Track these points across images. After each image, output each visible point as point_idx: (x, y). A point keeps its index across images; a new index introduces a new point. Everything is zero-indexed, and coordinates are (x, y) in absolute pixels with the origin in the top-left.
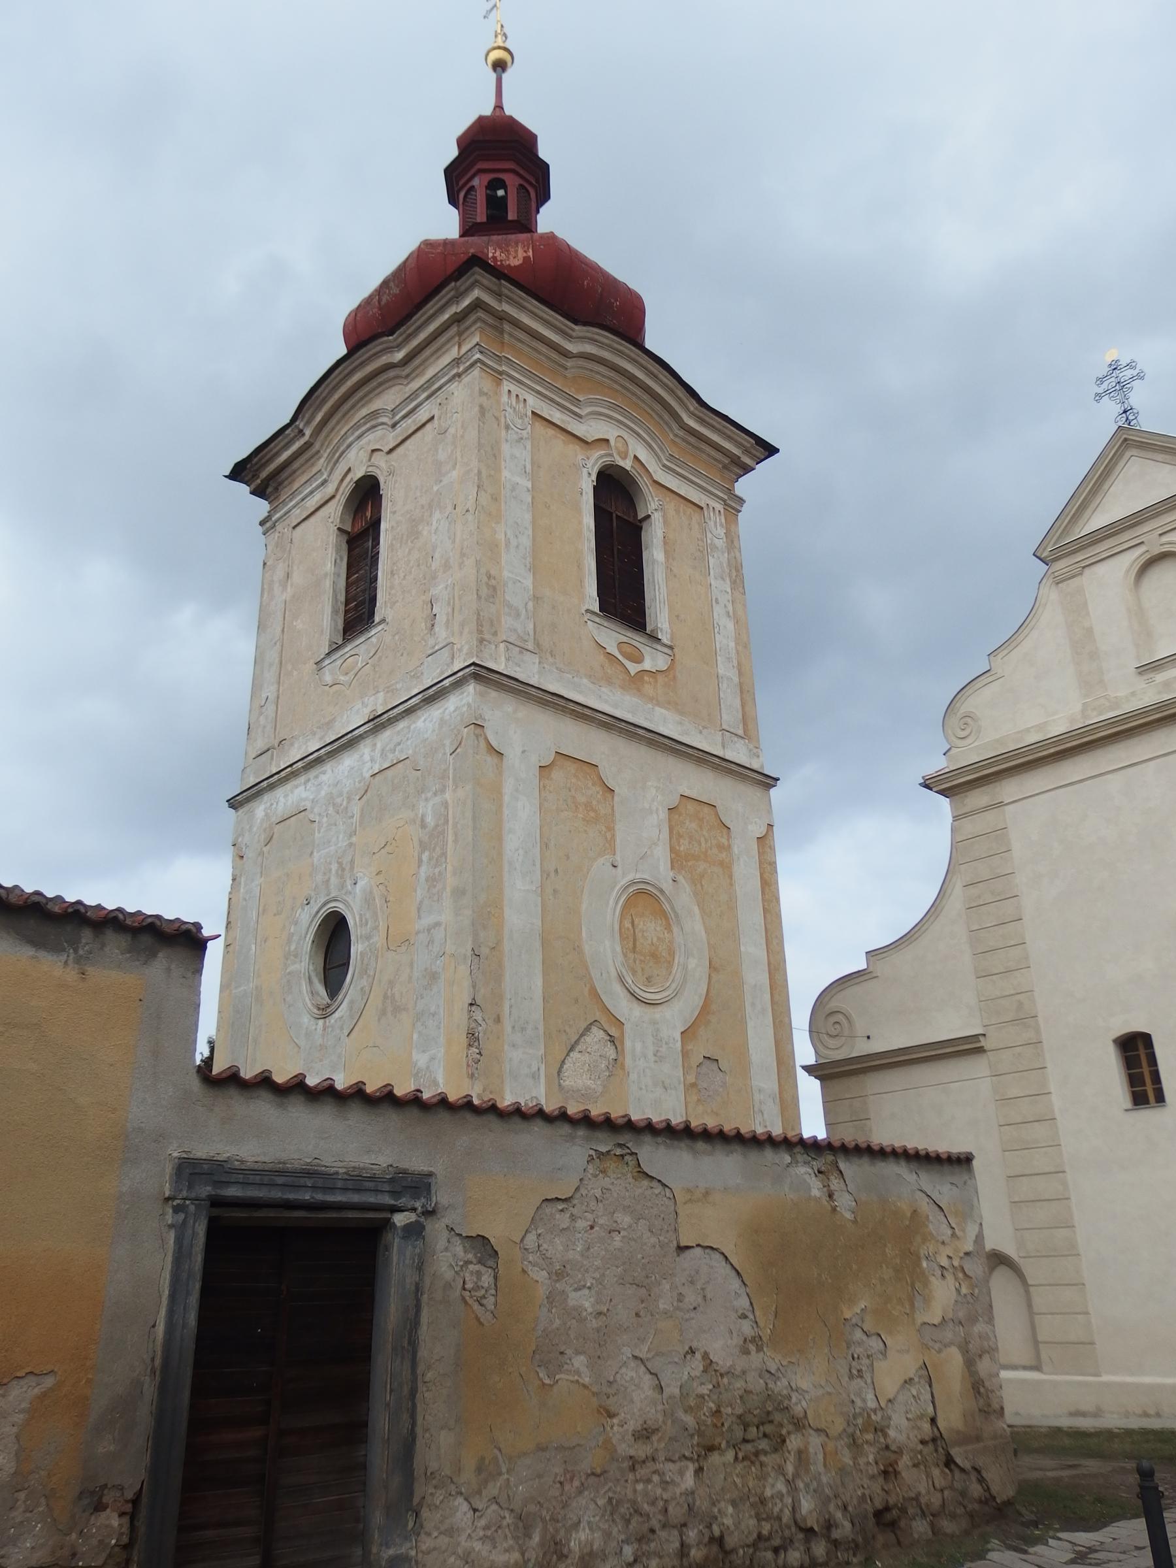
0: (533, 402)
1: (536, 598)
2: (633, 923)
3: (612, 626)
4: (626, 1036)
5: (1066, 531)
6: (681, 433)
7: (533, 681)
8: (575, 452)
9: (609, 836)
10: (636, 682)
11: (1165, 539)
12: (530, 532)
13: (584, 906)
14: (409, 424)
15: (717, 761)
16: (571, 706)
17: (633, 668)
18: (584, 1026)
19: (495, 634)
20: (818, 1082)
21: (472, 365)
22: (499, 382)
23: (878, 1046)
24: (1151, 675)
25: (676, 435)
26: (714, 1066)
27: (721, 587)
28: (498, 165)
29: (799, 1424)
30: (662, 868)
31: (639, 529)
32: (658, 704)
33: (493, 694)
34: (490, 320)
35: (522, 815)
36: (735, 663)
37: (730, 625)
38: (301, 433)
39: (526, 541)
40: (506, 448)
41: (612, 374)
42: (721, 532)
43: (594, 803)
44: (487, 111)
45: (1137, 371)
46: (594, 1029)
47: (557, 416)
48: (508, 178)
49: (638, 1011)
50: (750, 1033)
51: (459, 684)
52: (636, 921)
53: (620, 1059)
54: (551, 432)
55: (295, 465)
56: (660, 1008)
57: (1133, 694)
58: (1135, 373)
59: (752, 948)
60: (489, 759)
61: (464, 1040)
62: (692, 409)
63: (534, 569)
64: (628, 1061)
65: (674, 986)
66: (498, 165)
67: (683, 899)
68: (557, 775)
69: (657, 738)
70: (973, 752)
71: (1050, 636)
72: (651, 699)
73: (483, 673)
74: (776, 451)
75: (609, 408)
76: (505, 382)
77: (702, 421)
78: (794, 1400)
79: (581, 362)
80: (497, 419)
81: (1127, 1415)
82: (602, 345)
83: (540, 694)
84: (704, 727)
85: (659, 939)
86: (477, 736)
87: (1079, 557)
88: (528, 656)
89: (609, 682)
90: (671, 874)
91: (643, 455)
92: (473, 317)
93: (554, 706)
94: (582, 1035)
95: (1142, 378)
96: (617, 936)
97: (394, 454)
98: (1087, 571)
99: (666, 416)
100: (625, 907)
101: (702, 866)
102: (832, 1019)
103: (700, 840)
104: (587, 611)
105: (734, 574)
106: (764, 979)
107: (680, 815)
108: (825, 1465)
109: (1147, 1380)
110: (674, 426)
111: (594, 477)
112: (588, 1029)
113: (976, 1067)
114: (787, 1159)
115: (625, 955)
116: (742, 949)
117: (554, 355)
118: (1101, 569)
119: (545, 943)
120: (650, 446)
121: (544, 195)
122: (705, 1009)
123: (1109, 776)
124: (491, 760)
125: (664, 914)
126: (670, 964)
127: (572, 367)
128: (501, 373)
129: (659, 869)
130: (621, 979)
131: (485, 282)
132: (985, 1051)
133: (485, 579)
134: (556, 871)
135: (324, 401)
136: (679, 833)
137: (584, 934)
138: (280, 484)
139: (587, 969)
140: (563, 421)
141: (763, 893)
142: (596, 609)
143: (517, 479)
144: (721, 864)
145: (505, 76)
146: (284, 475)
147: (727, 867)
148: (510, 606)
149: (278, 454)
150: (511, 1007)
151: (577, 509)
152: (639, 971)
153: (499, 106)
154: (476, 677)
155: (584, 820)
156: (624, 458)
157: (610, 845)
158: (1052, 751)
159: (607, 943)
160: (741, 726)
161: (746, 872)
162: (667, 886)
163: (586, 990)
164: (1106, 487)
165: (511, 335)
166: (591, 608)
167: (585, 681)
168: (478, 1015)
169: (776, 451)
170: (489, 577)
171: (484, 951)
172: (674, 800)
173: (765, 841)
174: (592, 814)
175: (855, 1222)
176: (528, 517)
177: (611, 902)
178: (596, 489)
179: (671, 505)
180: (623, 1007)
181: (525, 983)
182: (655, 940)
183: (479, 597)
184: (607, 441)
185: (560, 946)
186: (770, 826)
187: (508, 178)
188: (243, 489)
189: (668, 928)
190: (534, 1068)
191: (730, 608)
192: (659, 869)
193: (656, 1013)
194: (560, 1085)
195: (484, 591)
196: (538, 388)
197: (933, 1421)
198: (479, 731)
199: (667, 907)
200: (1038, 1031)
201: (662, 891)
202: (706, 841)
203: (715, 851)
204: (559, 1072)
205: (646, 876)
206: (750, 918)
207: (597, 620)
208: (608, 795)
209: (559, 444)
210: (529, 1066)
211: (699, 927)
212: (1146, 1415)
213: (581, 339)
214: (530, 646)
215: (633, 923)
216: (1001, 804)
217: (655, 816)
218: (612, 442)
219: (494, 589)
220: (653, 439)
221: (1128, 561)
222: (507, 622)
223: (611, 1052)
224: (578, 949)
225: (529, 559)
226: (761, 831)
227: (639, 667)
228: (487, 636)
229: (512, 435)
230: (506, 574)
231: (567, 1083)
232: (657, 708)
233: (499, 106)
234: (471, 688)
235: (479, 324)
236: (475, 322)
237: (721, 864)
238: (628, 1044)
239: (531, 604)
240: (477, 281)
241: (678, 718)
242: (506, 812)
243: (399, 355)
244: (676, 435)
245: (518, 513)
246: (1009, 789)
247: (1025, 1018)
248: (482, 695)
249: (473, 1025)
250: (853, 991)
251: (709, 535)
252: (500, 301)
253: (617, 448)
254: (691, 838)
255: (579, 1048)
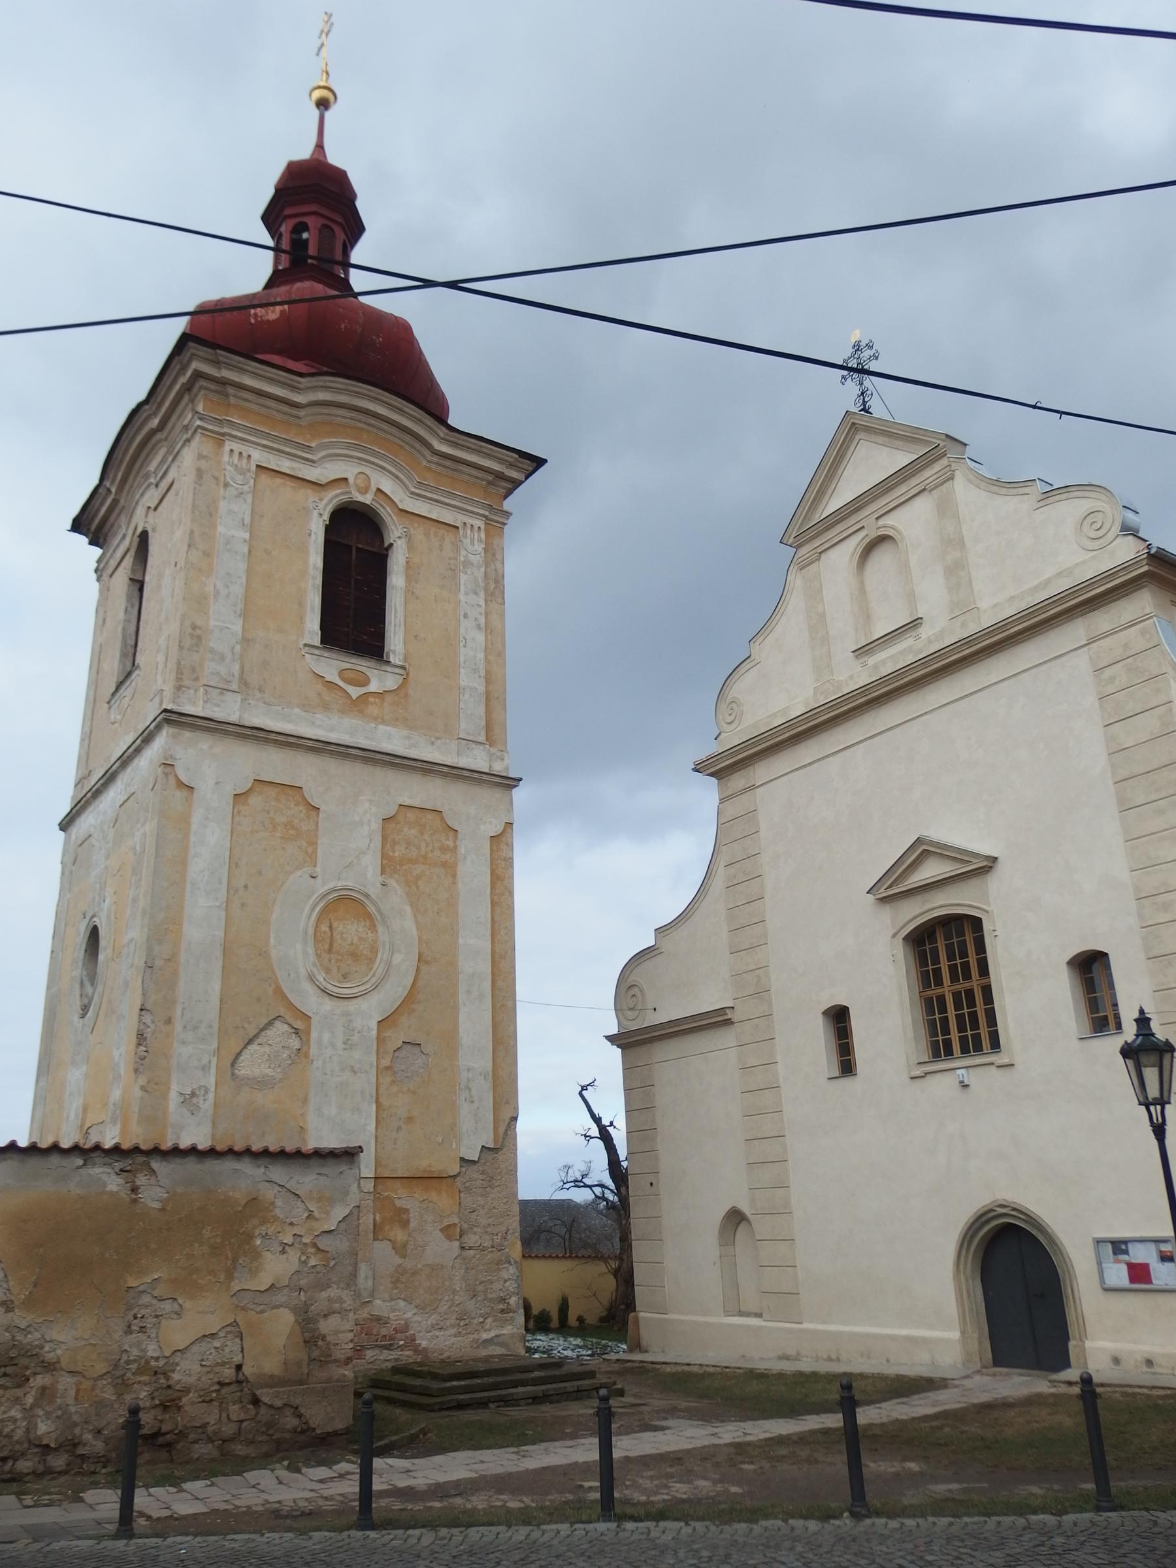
0: (258, 456)
1: (246, 641)
2: (331, 927)
3: (334, 656)
4: (313, 1028)
5: (807, 517)
6: (435, 459)
7: (234, 718)
8: (308, 497)
9: (310, 850)
10: (358, 705)
11: (881, 522)
12: (244, 581)
13: (274, 916)
14: (164, 485)
15: (445, 769)
16: (273, 736)
17: (354, 692)
18: (264, 1021)
19: (197, 679)
20: (620, 1050)
21: (195, 431)
22: (220, 443)
23: (662, 1017)
24: (865, 659)
25: (429, 462)
26: (416, 1050)
27: (471, 602)
28: (314, 208)
29: (50, 1367)
30: (369, 875)
31: (386, 556)
32: (384, 722)
33: (187, 734)
34: (213, 386)
35: (210, 839)
36: (483, 673)
37: (481, 638)
38: (109, 491)
39: (238, 590)
40: (223, 505)
41: (354, 415)
42: (479, 547)
43: (296, 821)
44: (303, 152)
45: (874, 351)
46: (278, 1024)
47: (286, 465)
48: (310, 220)
49: (328, 1005)
50: (462, 1018)
51: (158, 728)
52: (335, 925)
53: (305, 1049)
54: (279, 481)
55: (112, 518)
56: (355, 1001)
57: (851, 677)
58: (871, 353)
59: (473, 942)
60: (178, 793)
61: (134, 1041)
62: (442, 435)
63: (245, 615)
64: (313, 1050)
65: (374, 980)
66: (314, 208)
67: (394, 902)
68: (255, 800)
69: (372, 755)
70: (732, 739)
71: (792, 625)
72: (375, 719)
73: (175, 717)
74: (545, 461)
75: (348, 448)
76: (227, 443)
77: (455, 445)
78: (47, 1349)
79: (316, 409)
80: (216, 479)
81: (817, 1359)
82: (338, 391)
83: (238, 730)
84: (437, 738)
85: (360, 939)
86: (166, 775)
87: (817, 542)
88: (229, 697)
89: (326, 707)
90: (380, 879)
91: (388, 486)
92: (197, 386)
93: (256, 738)
94: (262, 1030)
95: (877, 358)
96: (311, 942)
97: (160, 508)
98: (823, 556)
99: (418, 445)
100: (325, 911)
101: (419, 869)
102: (631, 993)
103: (416, 848)
104: (305, 645)
105: (492, 586)
106: (486, 967)
107: (398, 823)
108: (76, 1399)
109: (832, 1328)
110: (427, 453)
111: (326, 517)
112: (270, 1023)
113: (725, 1039)
114: (80, 1162)
115: (318, 956)
116: (461, 941)
117: (286, 408)
118: (833, 554)
119: (227, 951)
120: (397, 477)
121: (355, 229)
122: (410, 999)
123: (831, 759)
124: (179, 794)
125: (369, 916)
126: (371, 961)
127: (306, 415)
128: (223, 434)
129: (366, 874)
130: (311, 978)
131: (201, 353)
132: (732, 1023)
133: (190, 630)
134: (246, 887)
135: (121, 462)
136: (394, 840)
137: (272, 941)
138: (106, 535)
139: (273, 971)
140: (293, 469)
141: (493, 887)
142: (317, 641)
143: (233, 532)
144: (444, 864)
145: (328, 115)
146: (108, 524)
147: (450, 869)
148: (212, 651)
149: (98, 510)
150: (184, 1009)
151: (304, 550)
152: (335, 970)
153: (320, 146)
154: (168, 721)
155: (282, 838)
156: (365, 491)
157: (311, 858)
158: (787, 735)
159: (299, 946)
160: (483, 733)
161: (473, 871)
162: (374, 891)
163: (270, 991)
164: (840, 472)
165: (234, 396)
166: (310, 642)
167: (297, 710)
168: (148, 1018)
169: (545, 461)
170: (194, 627)
171: (159, 963)
172: (391, 810)
173: (501, 841)
174: (292, 832)
175: (163, 1210)
176: (242, 566)
177: (307, 910)
178: (328, 530)
179: (418, 532)
180: (311, 1002)
181: (202, 988)
182: (355, 940)
183: (181, 648)
184: (346, 479)
185: (243, 955)
186: (509, 825)
187: (310, 220)
188: (82, 540)
189: (373, 928)
190: (205, 1061)
191: (482, 620)
192: (366, 874)
193: (352, 1006)
194: (233, 1075)
195: (188, 642)
196: (264, 442)
197: (239, 1367)
198: (168, 769)
199: (372, 909)
200: (770, 1005)
201: (367, 896)
202: (427, 845)
203: (437, 853)
204: (233, 1064)
205: (350, 884)
206: (474, 912)
207: (316, 652)
208: (313, 813)
209: (288, 491)
210: (200, 1060)
211: (409, 924)
212: (830, 1359)
213: (314, 388)
214: (234, 687)
215: (331, 927)
216: (753, 787)
217: (366, 827)
218: (351, 481)
219: (199, 638)
220: (399, 470)
221: (853, 545)
222: (210, 666)
223: (295, 1043)
224: (264, 954)
225: (240, 606)
226: (496, 829)
227: (363, 690)
228: (187, 683)
229: (231, 492)
230: (212, 623)
231: (243, 1072)
232: (381, 727)
233: (320, 146)
234: (166, 731)
235: (203, 392)
236: (199, 391)
237: (444, 864)
238: (314, 1035)
239: (238, 648)
240: (193, 354)
241: (405, 733)
242: (192, 838)
243: (155, 422)
244: (429, 462)
245: (232, 565)
246: (762, 771)
247: (762, 993)
248: (174, 736)
249: (142, 1027)
250: (648, 965)
251: (463, 553)
252: (220, 368)
253: (356, 485)
254: (408, 843)
255: (259, 1040)
